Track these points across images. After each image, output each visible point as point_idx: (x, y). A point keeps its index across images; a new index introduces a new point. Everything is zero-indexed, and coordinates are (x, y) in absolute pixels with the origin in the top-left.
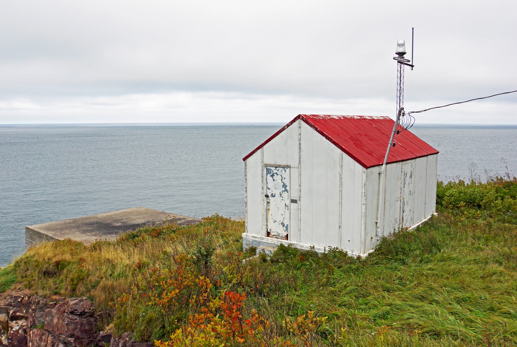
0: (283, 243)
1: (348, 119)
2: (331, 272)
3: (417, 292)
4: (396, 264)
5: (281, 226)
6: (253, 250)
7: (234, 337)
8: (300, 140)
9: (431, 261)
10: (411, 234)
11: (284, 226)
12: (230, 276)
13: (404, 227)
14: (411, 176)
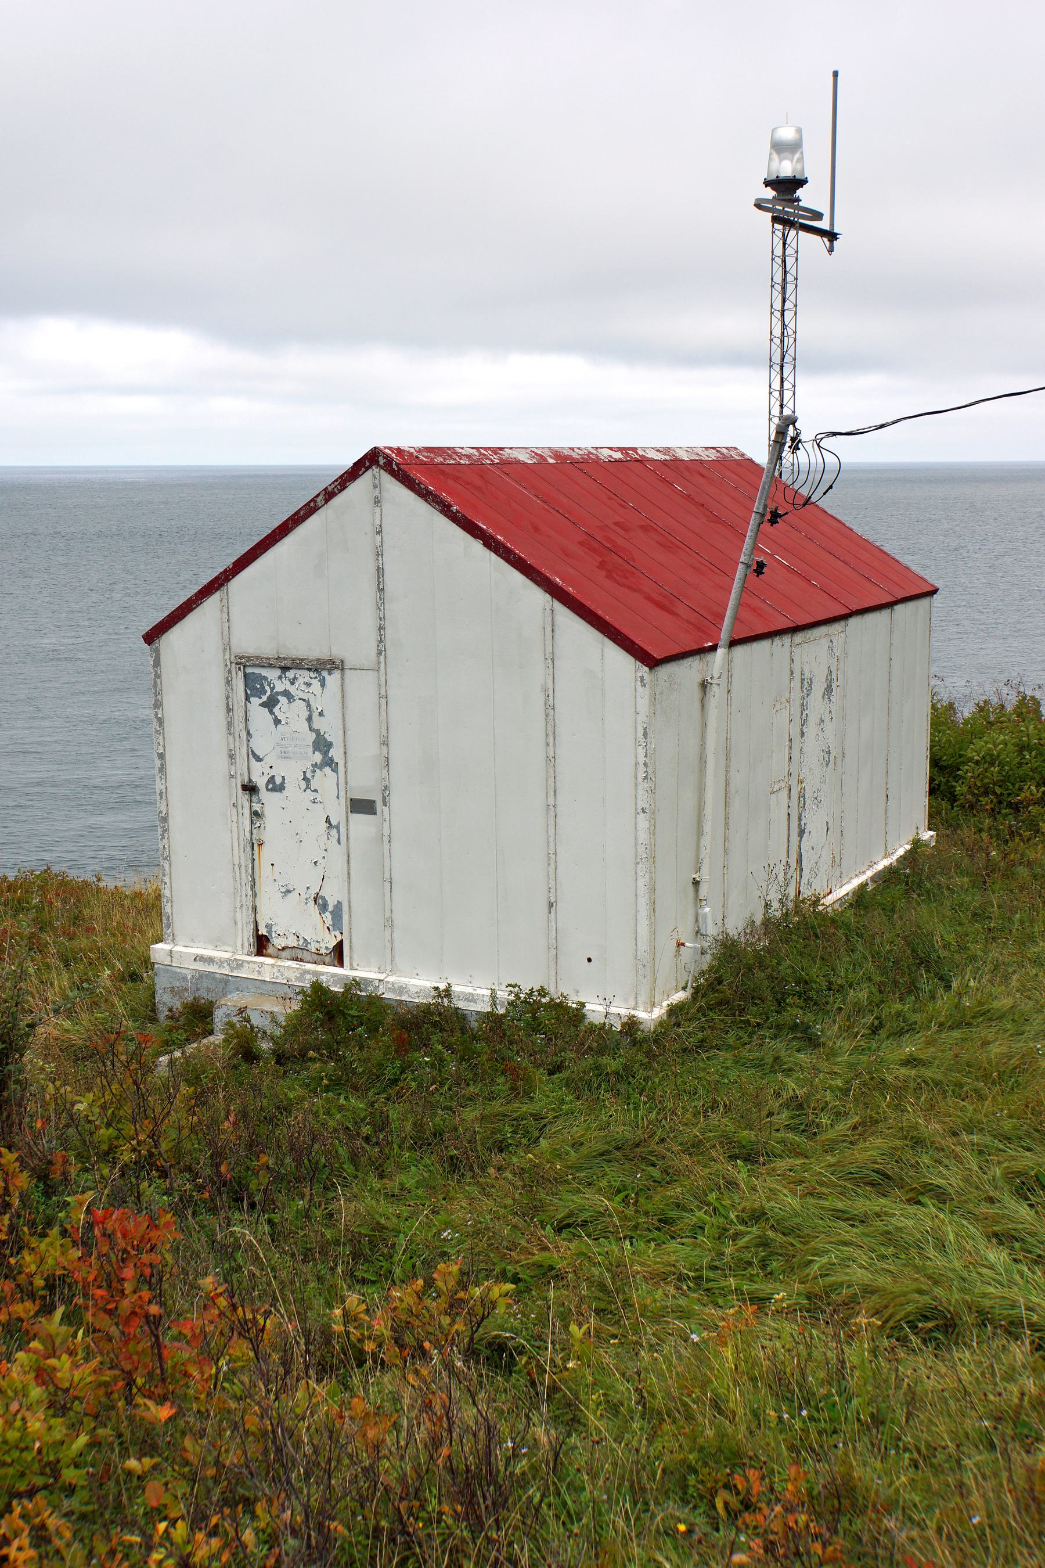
0: (323, 978)
1: (574, 462)
2: (522, 1089)
3: (861, 1157)
4: (778, 1046)
5: (313, 909)
6: (199, 1015)
7: (129, 1400)
8: (379, 554)
9: (911, 1028)
10: (833, 921)
11: (324, 908)
12: (105, 1133)
13: (806, 893)
14: (829, 689)
